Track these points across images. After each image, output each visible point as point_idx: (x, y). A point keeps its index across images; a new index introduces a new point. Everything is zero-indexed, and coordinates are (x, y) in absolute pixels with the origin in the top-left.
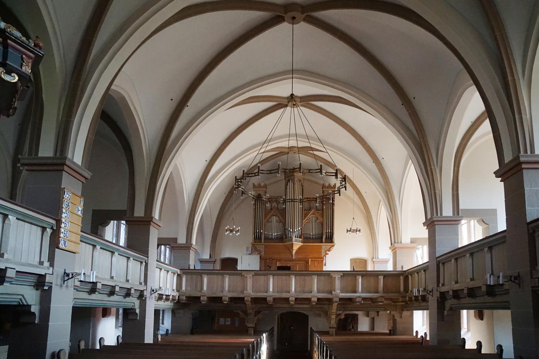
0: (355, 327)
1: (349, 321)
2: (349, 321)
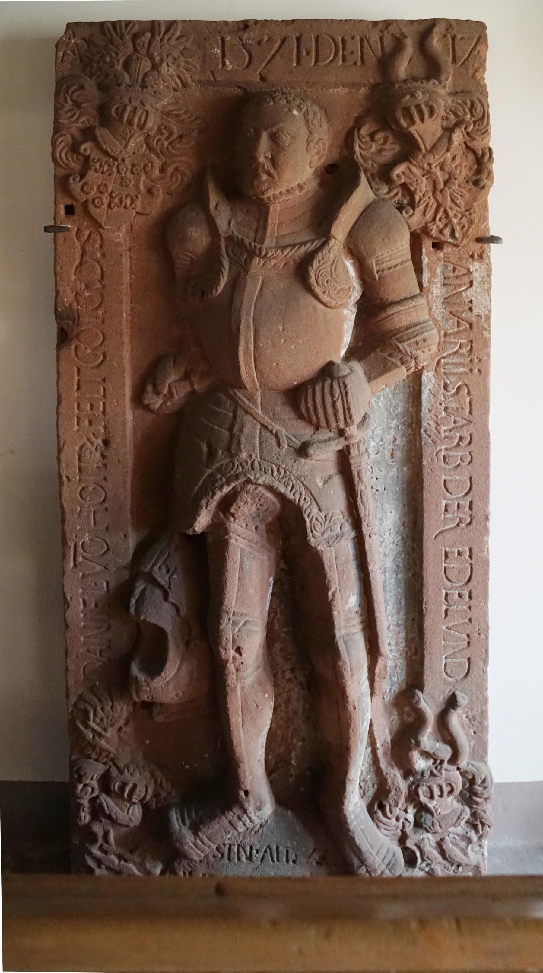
0: (423, 311)
1: (296, 175)
2: (296, 175)
